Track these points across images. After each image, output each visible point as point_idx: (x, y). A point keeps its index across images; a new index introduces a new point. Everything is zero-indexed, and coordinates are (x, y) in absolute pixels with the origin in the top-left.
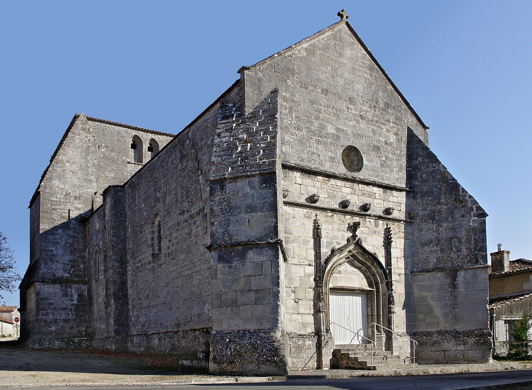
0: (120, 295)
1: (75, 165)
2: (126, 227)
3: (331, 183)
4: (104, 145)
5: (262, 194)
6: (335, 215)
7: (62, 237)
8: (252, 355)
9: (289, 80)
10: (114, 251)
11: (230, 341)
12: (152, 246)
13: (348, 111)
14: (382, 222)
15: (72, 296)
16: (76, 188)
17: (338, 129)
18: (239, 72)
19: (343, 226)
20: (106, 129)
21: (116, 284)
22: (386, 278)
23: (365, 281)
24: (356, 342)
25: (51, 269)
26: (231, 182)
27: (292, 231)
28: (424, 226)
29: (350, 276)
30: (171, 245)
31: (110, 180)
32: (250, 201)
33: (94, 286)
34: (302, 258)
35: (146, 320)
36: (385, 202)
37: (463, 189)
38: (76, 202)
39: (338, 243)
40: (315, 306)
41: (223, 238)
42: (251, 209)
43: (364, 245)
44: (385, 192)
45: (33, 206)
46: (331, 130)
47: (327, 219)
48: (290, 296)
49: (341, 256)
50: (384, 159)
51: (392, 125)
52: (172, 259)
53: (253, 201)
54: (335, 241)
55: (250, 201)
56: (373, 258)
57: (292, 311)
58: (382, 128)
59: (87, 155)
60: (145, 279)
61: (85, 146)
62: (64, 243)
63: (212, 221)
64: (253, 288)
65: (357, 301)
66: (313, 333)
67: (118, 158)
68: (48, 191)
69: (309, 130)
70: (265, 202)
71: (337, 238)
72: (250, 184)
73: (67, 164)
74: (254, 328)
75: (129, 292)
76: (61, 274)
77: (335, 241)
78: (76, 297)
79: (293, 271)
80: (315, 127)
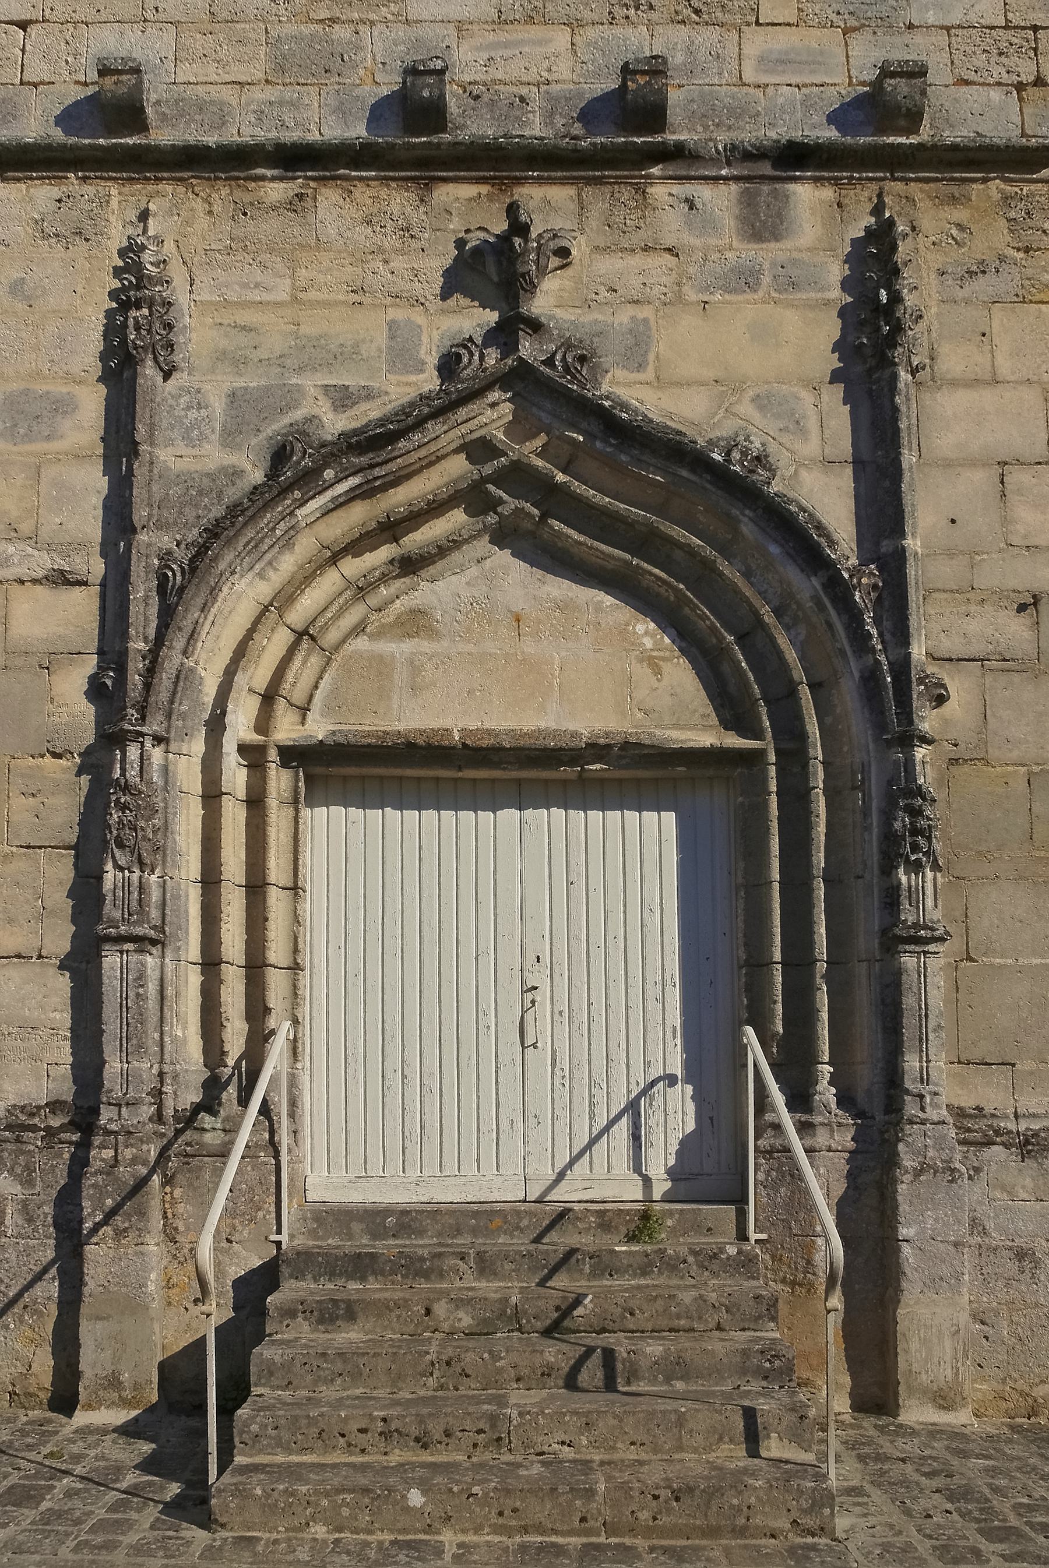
6: (329, 197)
7: (1027, 725)
14: (827, 193)
19: (399, 263)
23: (681, 677)
24: (611, 1180)
29: (529, 647)
36: (855, 40)
39: (343, 398)
40: (86, 893)
47: (249, 227)
54: (311, 383)
56: (729, 486)
65: (641, 849)
66: (55, 1106)
77: (311, 383)
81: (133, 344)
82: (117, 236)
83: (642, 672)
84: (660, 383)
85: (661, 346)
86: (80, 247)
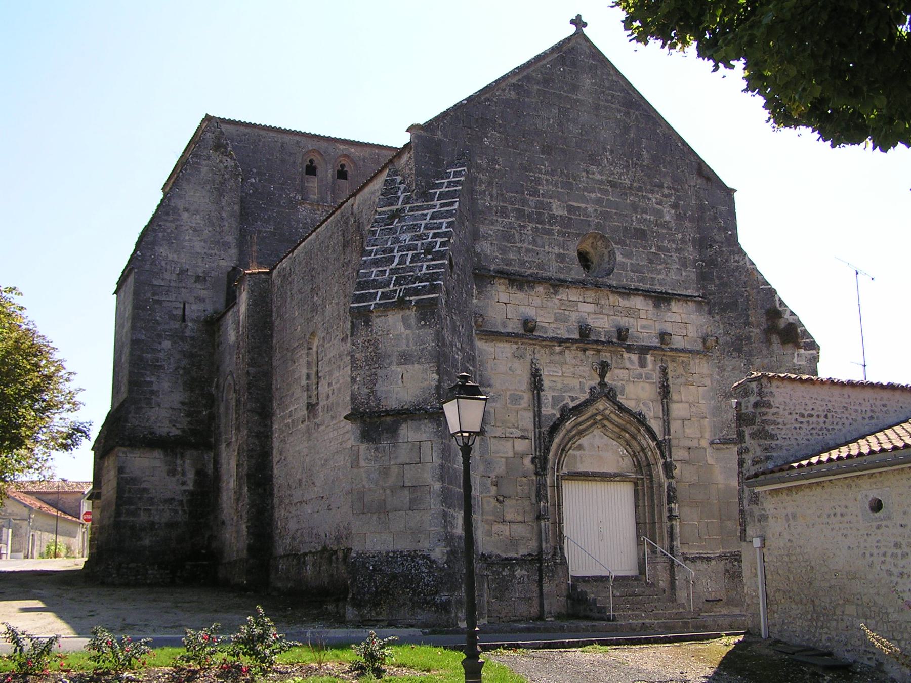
0: (260, 476)
1: (198, 217)
2: (272, 347)
3: (560, 297)
4: (255, 170)
5: (419, 337)
8: (403, 592)
9: (487, 137)
10: (250, 393)
11: (374, 569)
12: (308, 390)
13: (588, 177)
15: (184, 474)
16: (200, 260)
17: (571, 209)
18: (407, 131)
19: (581, 368)
20: (260, 140)
21: (252, 457)
22: (663, 456)
25: (148, 420)
26: (379, 316)
27: (492, 382)
28: (727, 363)
30: (330, 393)
31: (265, 237)
32: (404, 347)
33: (224, 455)
34: (510, 425)
35: (297, 527)
37: (780, 299)
38: (199, 286)
39: (573, 399)
41: (367, 404)
42: (405, 358)
43: (620, 398)
44: (657, 306)
45: (122, 291)
46: (558, 210)
47: (553, 358)
48: (489, 491)
49: (580, 420)
50: (653, 250)
51: (666, 191)
52: (333, 418)
53: (408, 345)
55: (404, 347)
56: (640, 419)
57: (491, 518)
58: (649, 199)
59: (221, 195)
60: (297, 449)
61: (218, 179)
62: (173, 366)
63: (354, 375)
64: (407, 484)
67: (281, 195)
68: (147, 267)
69: (520, 214)
70: (423, 349)
71: (572, 389)
72: (404, 320)
73: (185, 215)
74: (409, 548)
75: (275, 471)
76: (166, 430)
77: (566, 394)
78: (191, 475)
79: (493, 448)
80: (530, 207)
81: (536, 383)
82: (529, 358)
83: (620, 459)
84: (627, 399)
85: (627, 390)
86: (522, 360)
